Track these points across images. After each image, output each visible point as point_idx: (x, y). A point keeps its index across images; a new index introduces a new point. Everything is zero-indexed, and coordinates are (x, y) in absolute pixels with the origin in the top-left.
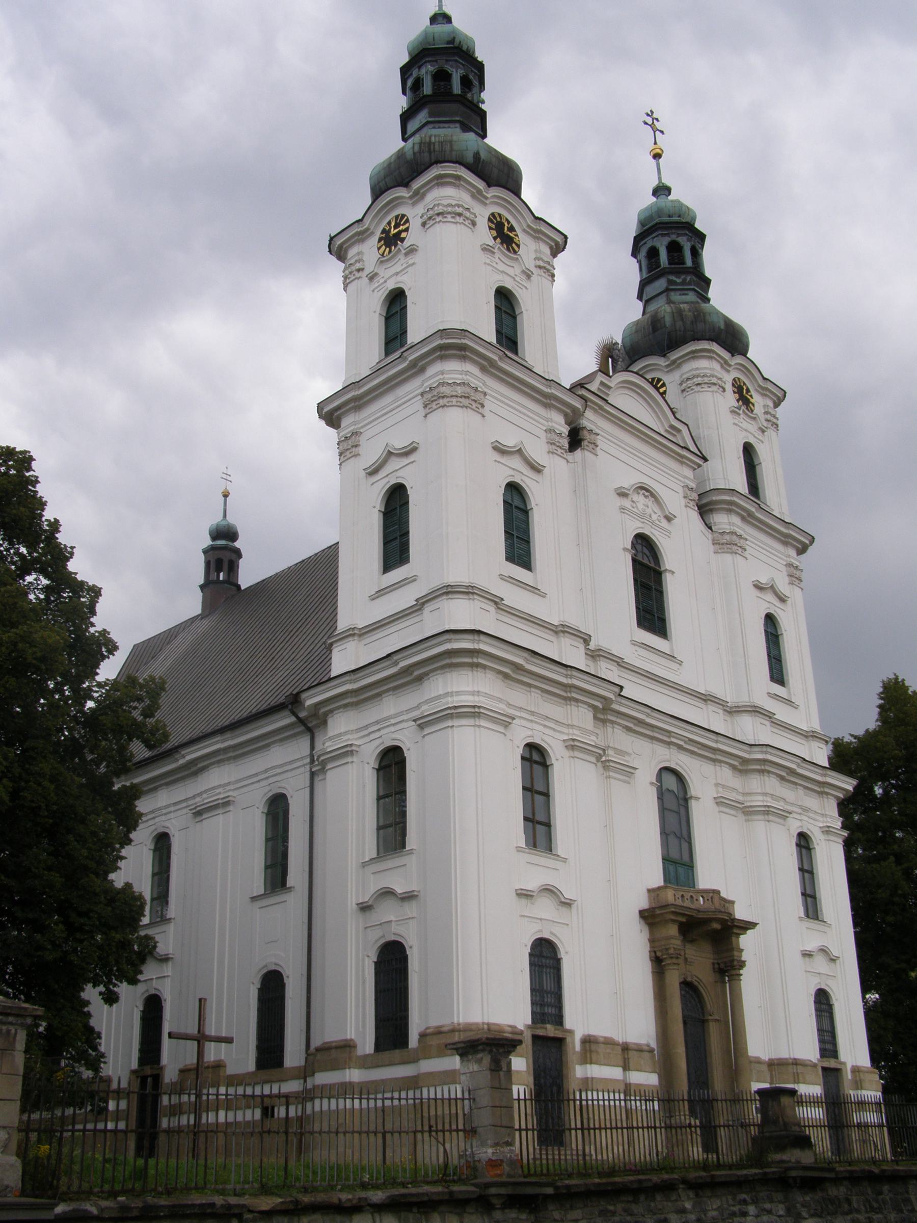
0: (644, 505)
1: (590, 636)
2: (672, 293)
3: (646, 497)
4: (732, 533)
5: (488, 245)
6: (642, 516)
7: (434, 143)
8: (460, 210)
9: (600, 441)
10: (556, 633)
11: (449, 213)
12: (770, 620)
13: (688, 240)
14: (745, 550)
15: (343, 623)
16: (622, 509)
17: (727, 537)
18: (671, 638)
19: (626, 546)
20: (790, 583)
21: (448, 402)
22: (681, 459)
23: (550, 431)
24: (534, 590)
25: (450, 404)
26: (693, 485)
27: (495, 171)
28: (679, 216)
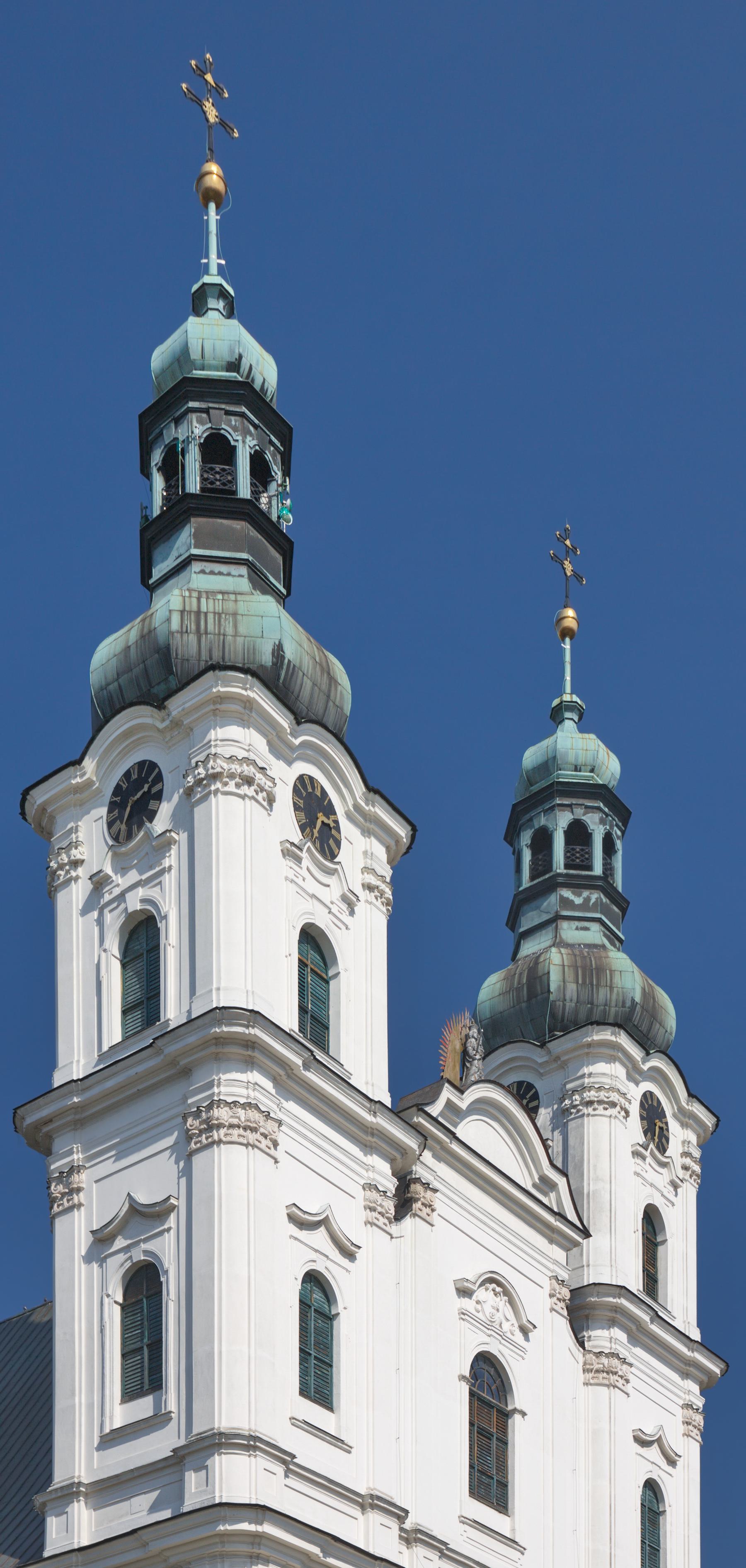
0: (493, 1308)
1: (407, 1512)
2: (565, 925)
3: (496, 1294)
4: (614, 1355)
5: (292, 844)
6: (489, 1326)
7: (206, 614)
8: (249, 770)
9: (438, 1201)
10: (363, 1507)
11: (232, 776)
12: (652, 1488)
13: (602, 822)
14: (627, 1381)
15: (60, 1477)
16: (463, 1313)
17: (605, 1361)
18: (513, 1513)
19: (464, 1374)
20: (684, 1435)
21: (226, 1135)
22: (551, 1234)
23: (370, 1187)
24: (336, 1441)
25: (228, 1139)
26: (564, 1275)
27: (308, 684)
28: (592, 771)
